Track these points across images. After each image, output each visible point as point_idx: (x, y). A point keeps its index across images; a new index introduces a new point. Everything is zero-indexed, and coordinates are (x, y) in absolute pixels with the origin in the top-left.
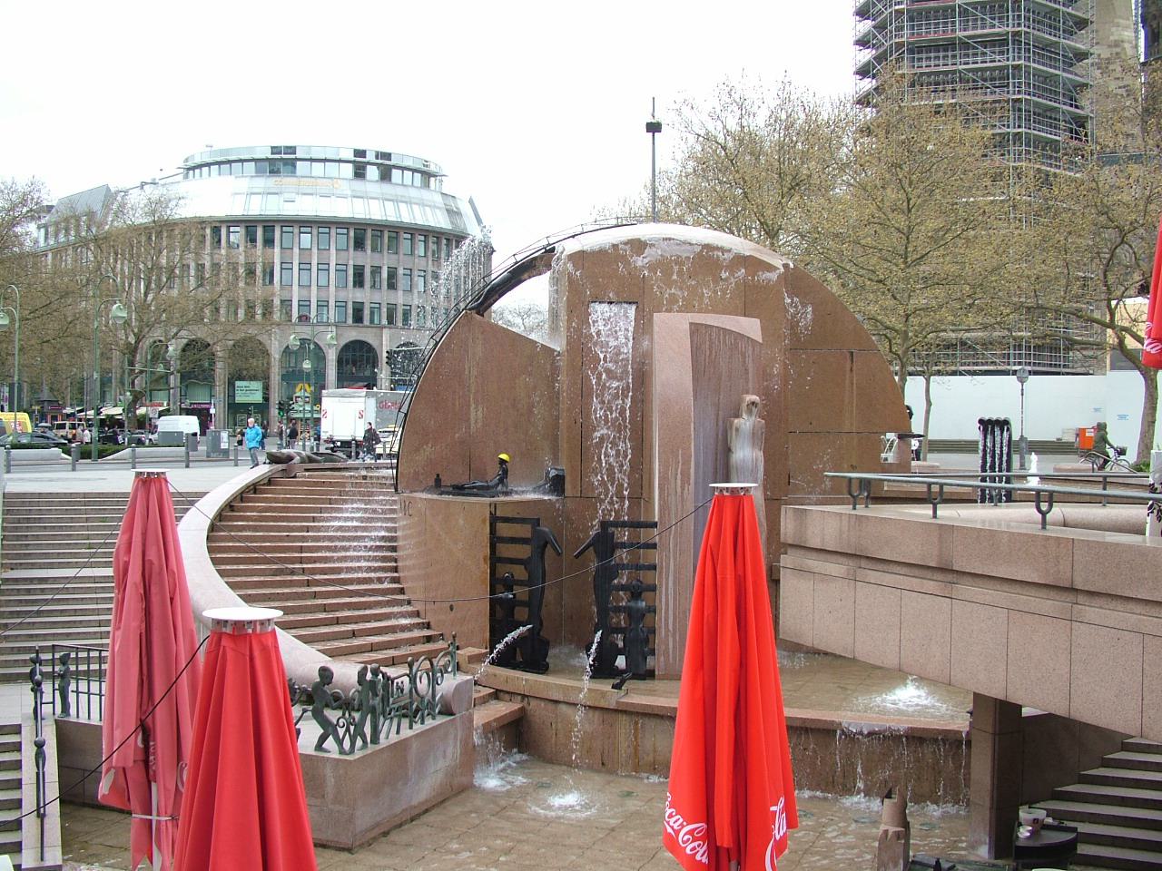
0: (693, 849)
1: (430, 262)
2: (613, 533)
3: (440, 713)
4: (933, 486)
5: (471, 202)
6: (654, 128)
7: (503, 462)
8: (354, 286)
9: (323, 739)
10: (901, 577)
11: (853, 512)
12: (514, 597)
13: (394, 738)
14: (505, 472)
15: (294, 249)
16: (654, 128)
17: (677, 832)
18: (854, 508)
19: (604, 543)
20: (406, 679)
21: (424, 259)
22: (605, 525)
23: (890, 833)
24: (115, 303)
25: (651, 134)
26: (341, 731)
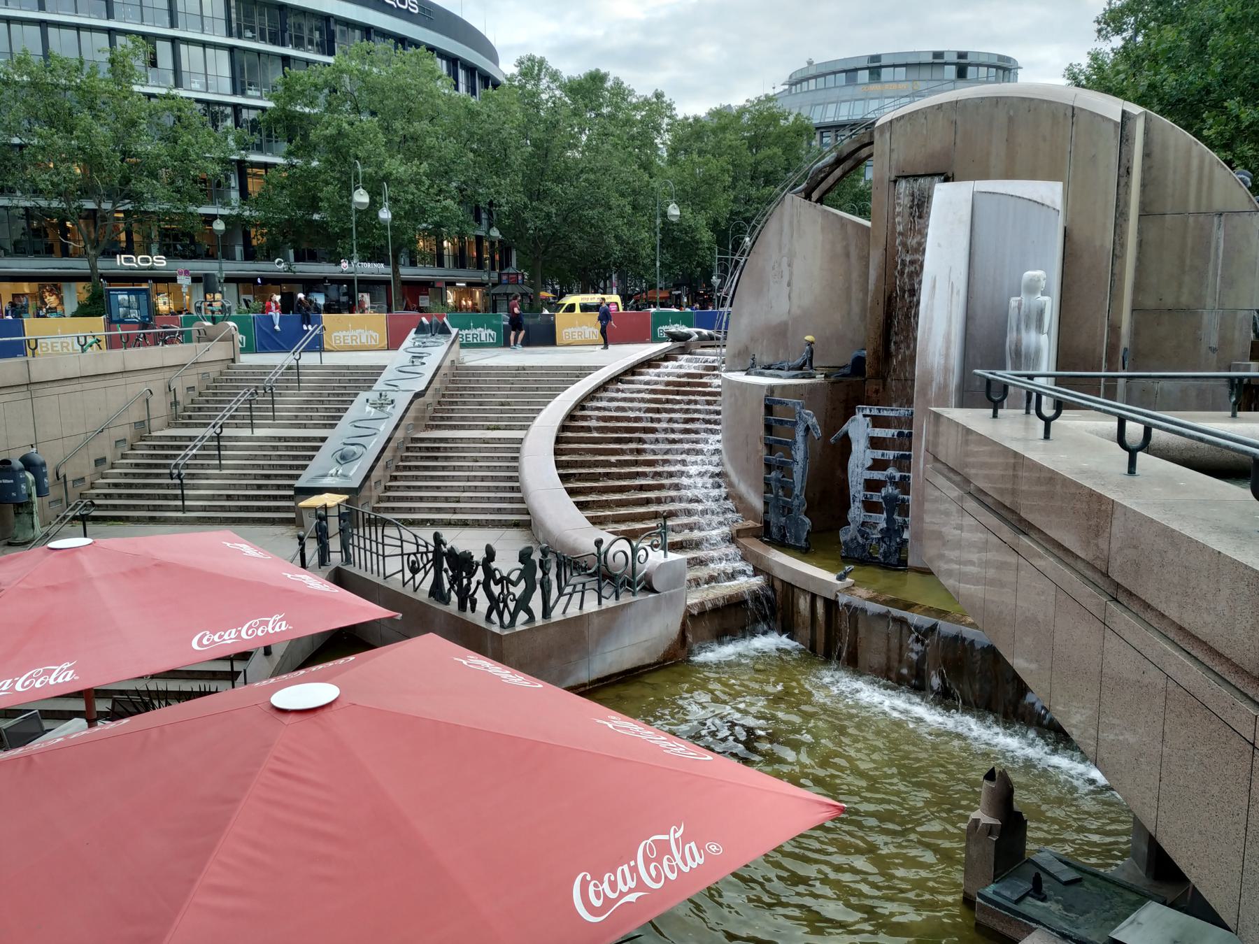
0: (672, 869)
4: (244, 111)
13: (573, 611)
17: (641, 885)
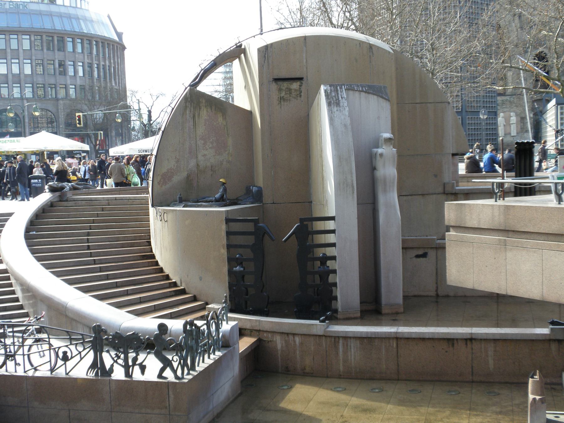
1: (86, 57)
2: (307, 225)
3: (222, 347)
5: (109, 17)
9: (162, 370)
11: (496, 203)
12: (244, 269)
15: (7, 49)
18: (496, 201)
20: (205, 327)
26: (175, 365)
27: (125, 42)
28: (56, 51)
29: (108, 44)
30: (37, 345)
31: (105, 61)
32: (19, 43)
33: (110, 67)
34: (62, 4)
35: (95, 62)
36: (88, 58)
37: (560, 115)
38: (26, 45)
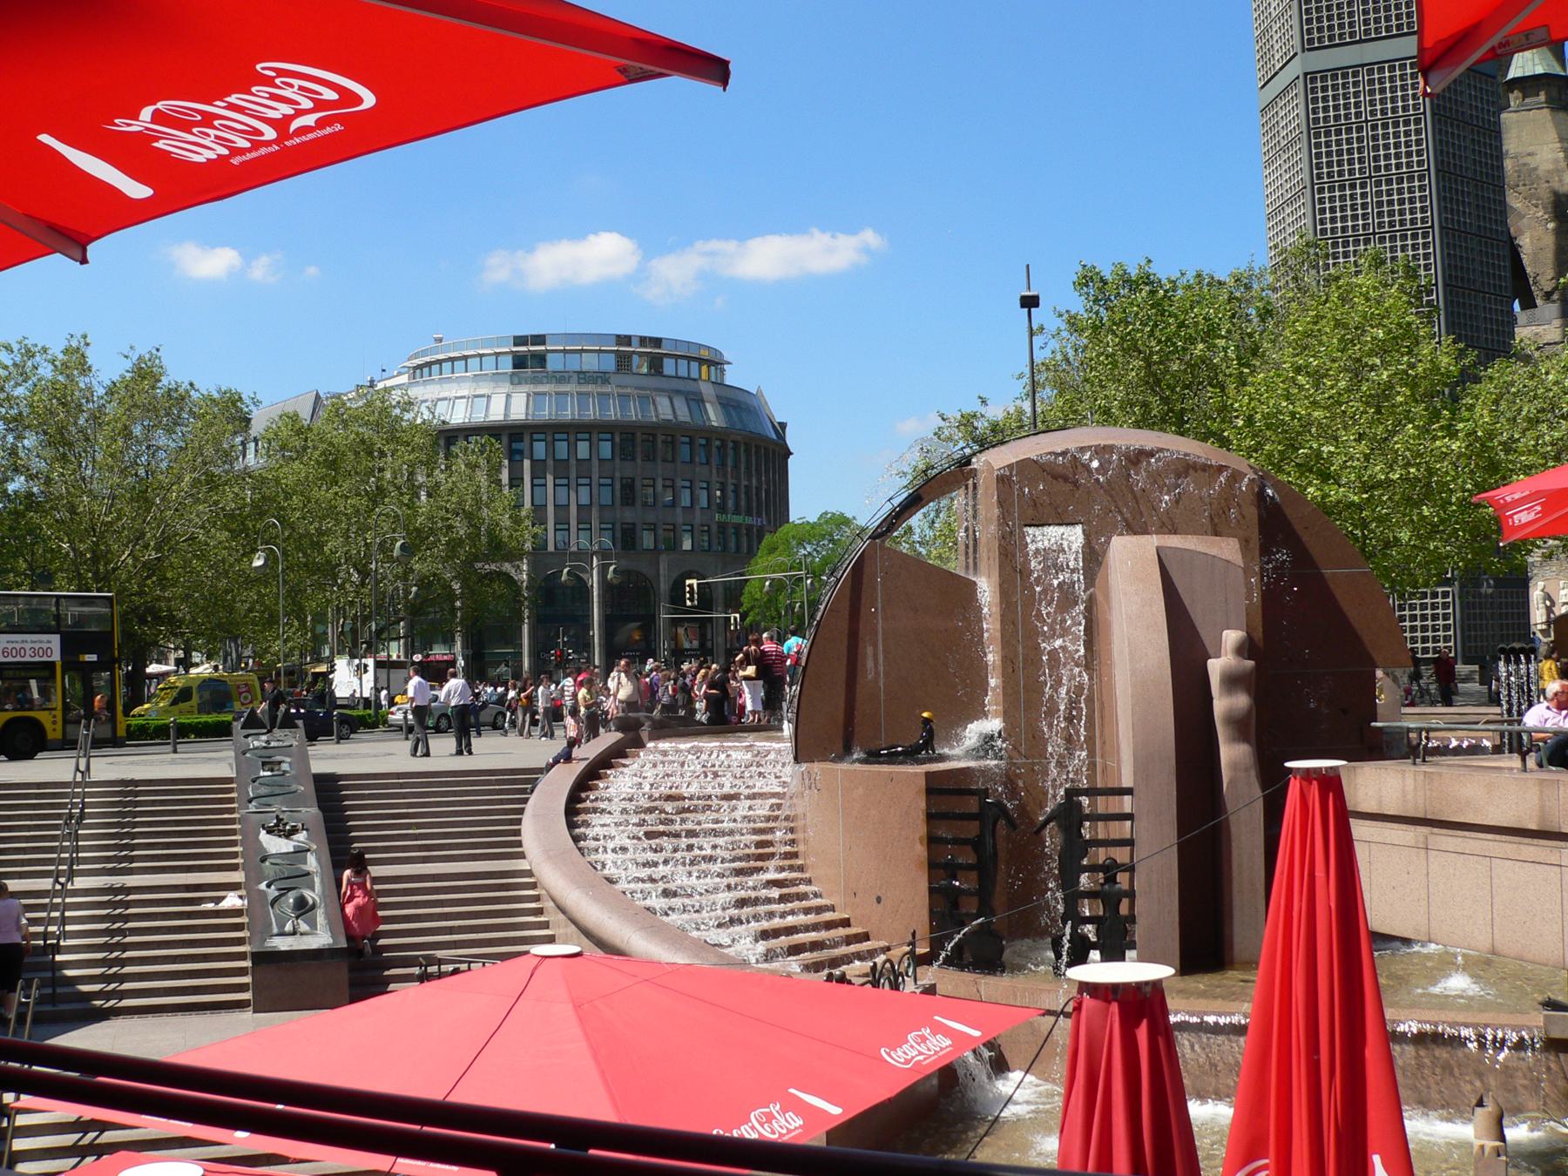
1: (714, 471)
6: (1030, 302)
7: (927, 721)
8: (622, 504)
10: (1491, 843)
14: (931, 734)
15: (571, 460)
16: (1030, 302)
19: (1070, 815)
21: (707, 467)
22: (1072, 793)
23: (1487, 1150)
24: (397, 541)
25: (1026, 310)
27: (791, 441)
28: (659, 462)
29: (756, 446)
30: (936, 1052)
31: (749, 480)
32: (573, 449)
33: (758, 489)
34: (674, 374)
35: (730, 481)
36: (718, 473)
37: (92, 591)
38: (606, 449)
